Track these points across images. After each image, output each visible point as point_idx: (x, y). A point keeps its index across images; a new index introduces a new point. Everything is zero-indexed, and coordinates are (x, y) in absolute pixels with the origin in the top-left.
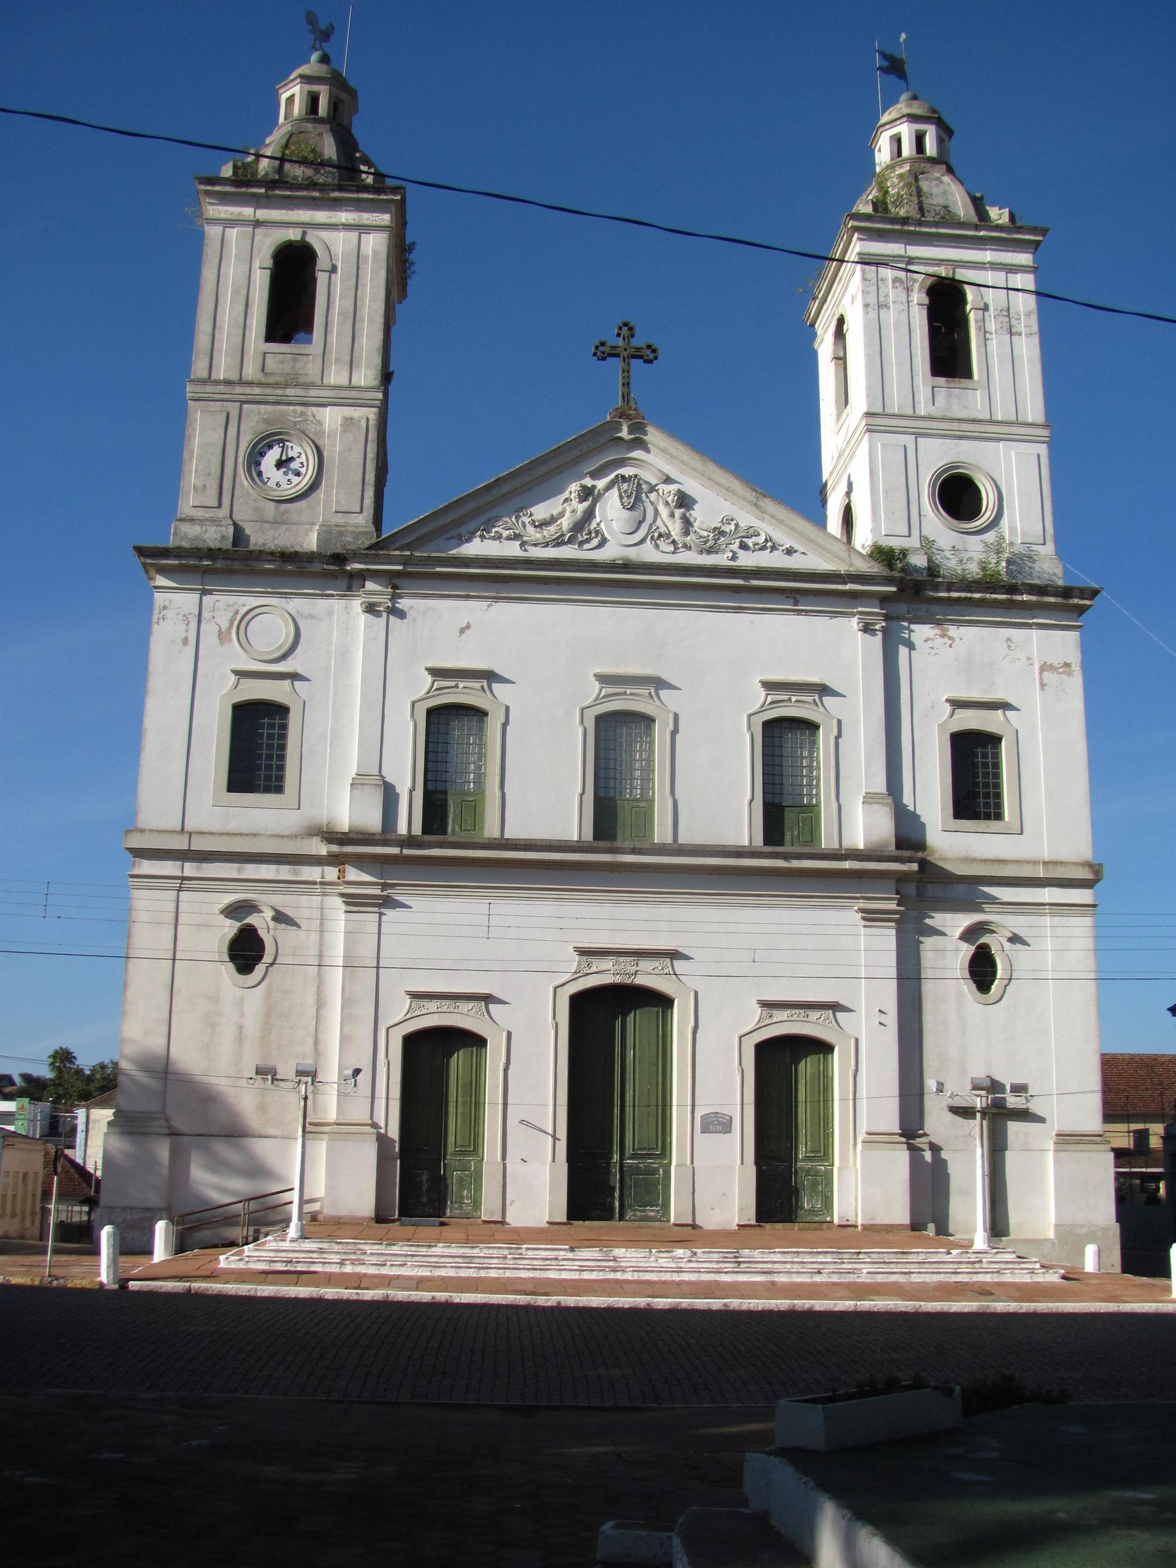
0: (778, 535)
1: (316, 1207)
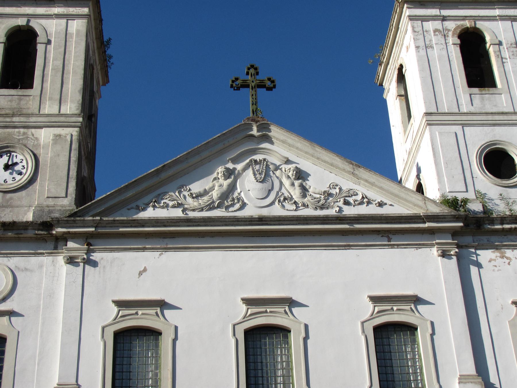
0: (371, 194)
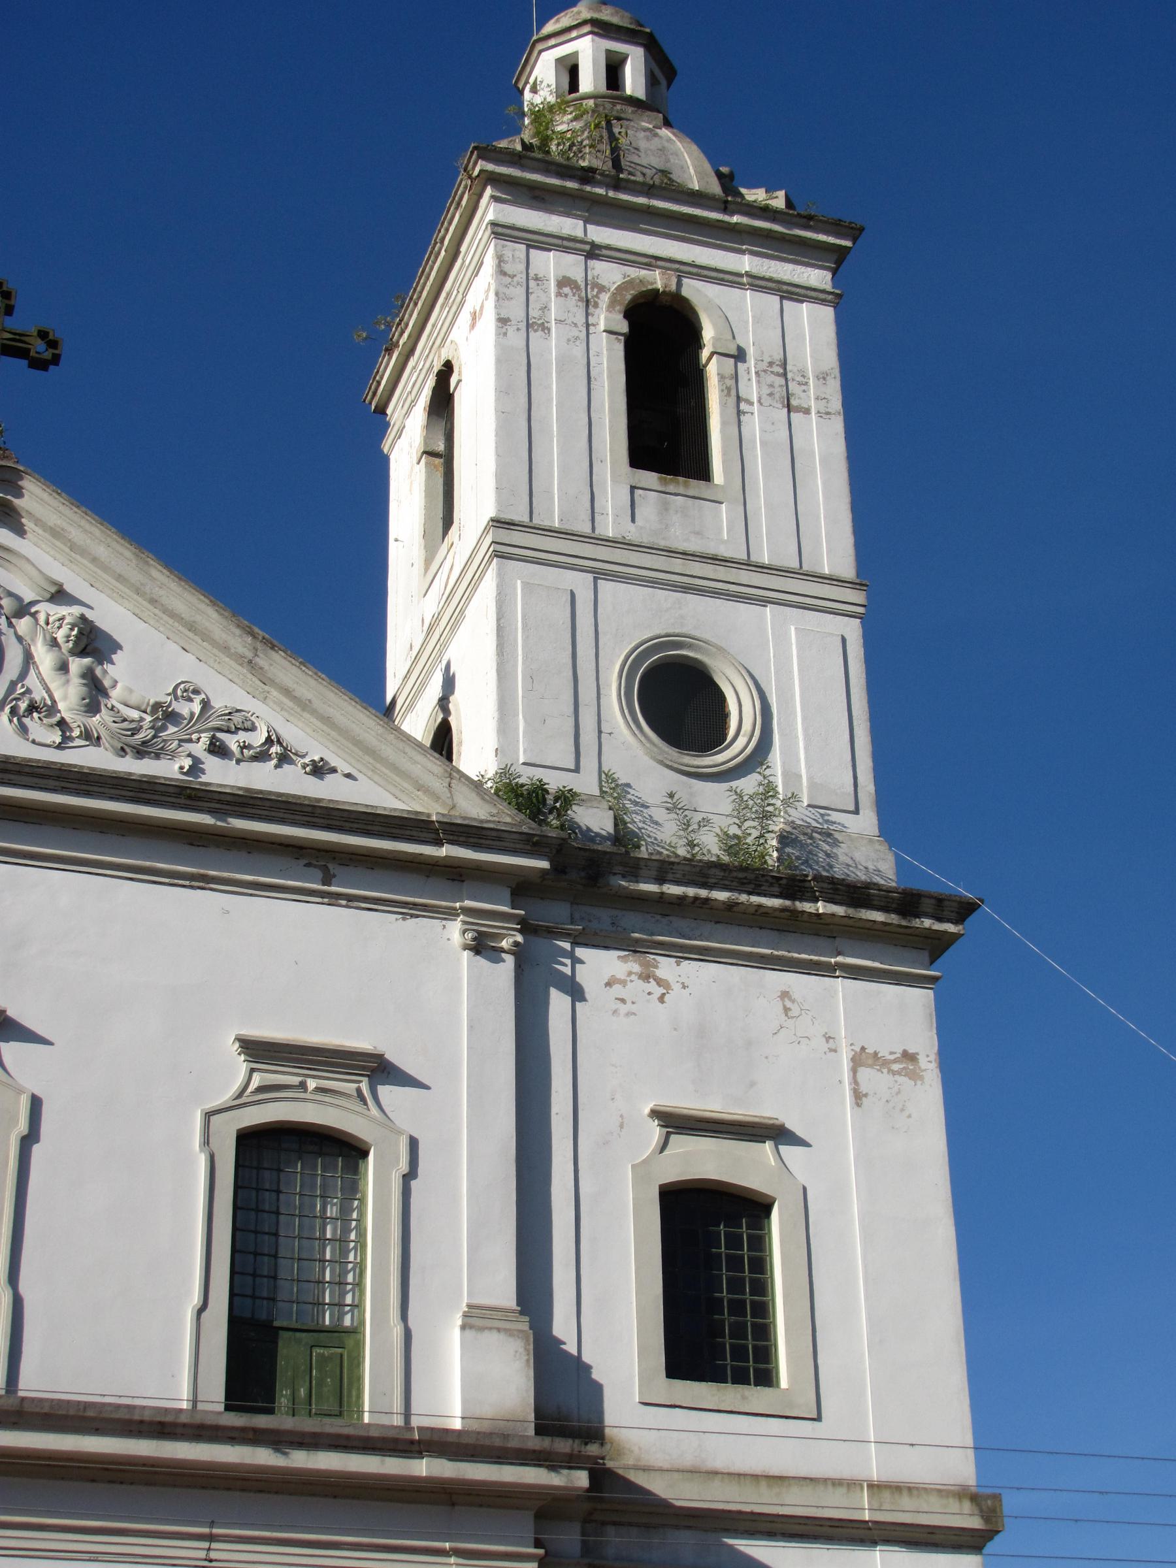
0: (294, 734)
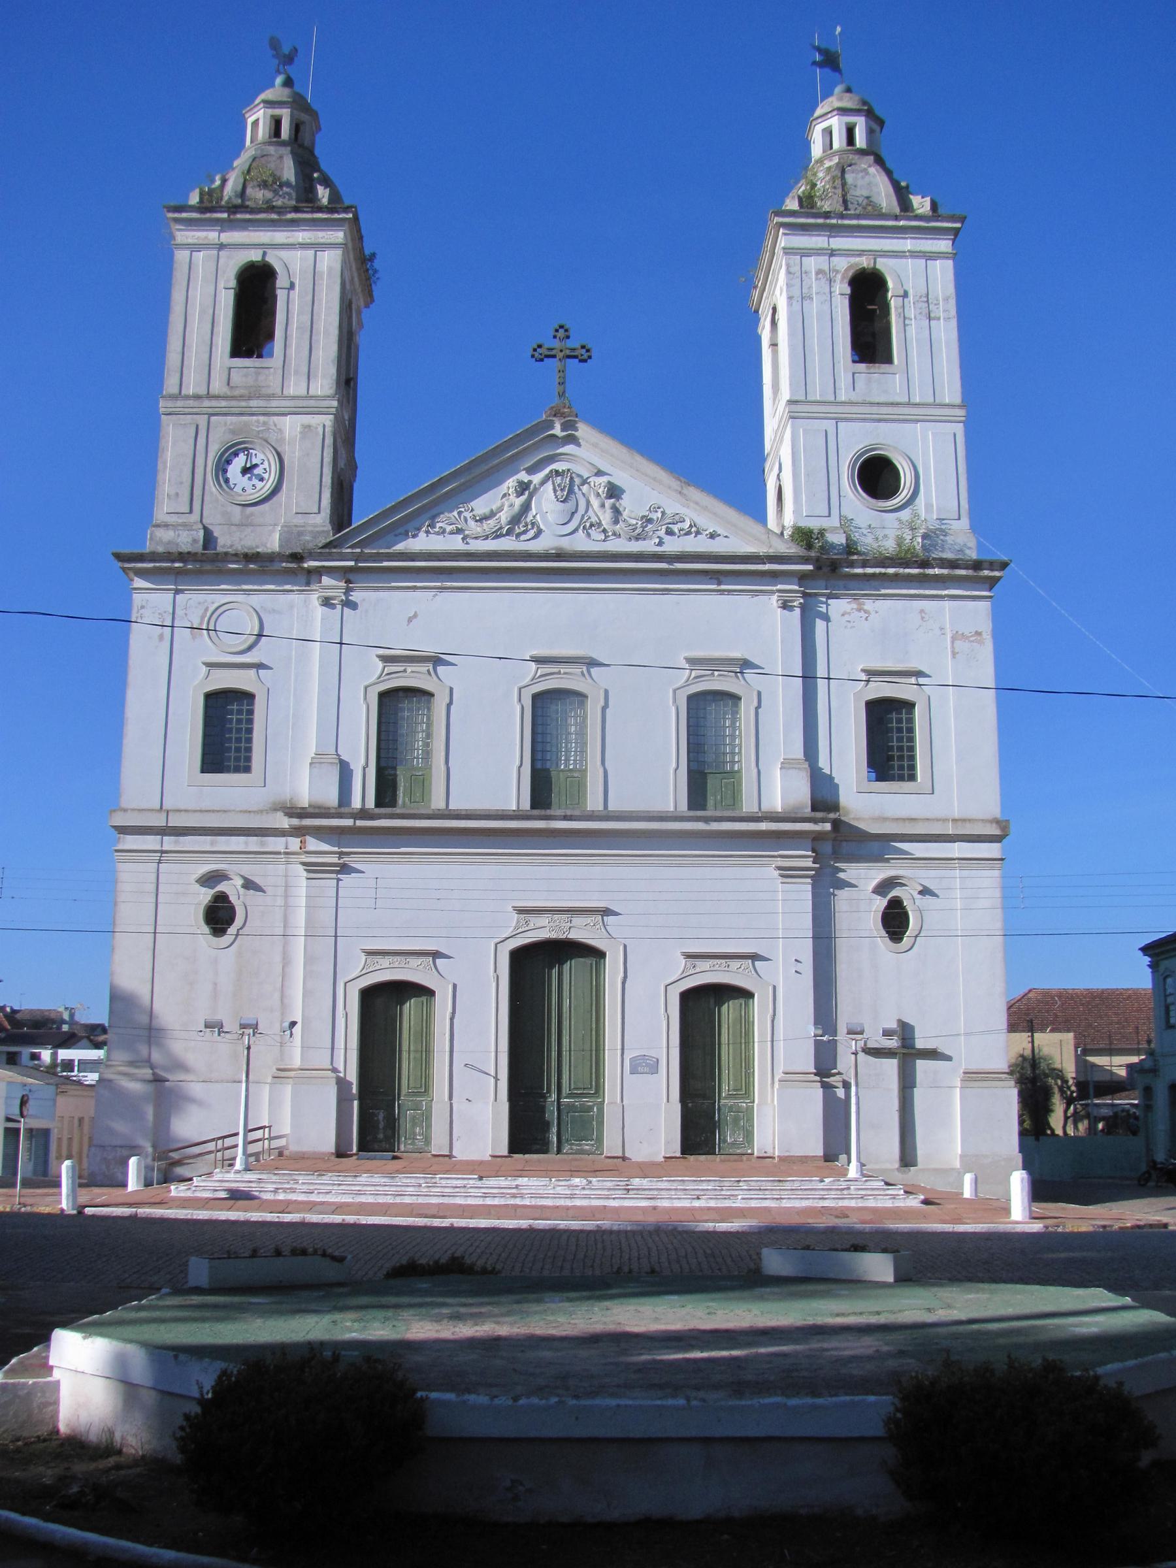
1: (281, 1142)
